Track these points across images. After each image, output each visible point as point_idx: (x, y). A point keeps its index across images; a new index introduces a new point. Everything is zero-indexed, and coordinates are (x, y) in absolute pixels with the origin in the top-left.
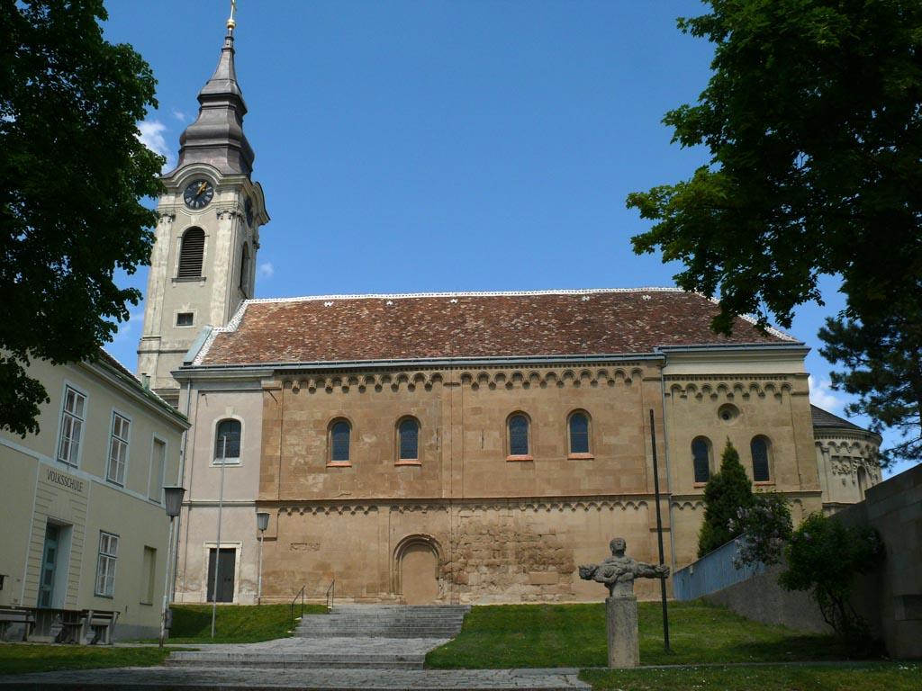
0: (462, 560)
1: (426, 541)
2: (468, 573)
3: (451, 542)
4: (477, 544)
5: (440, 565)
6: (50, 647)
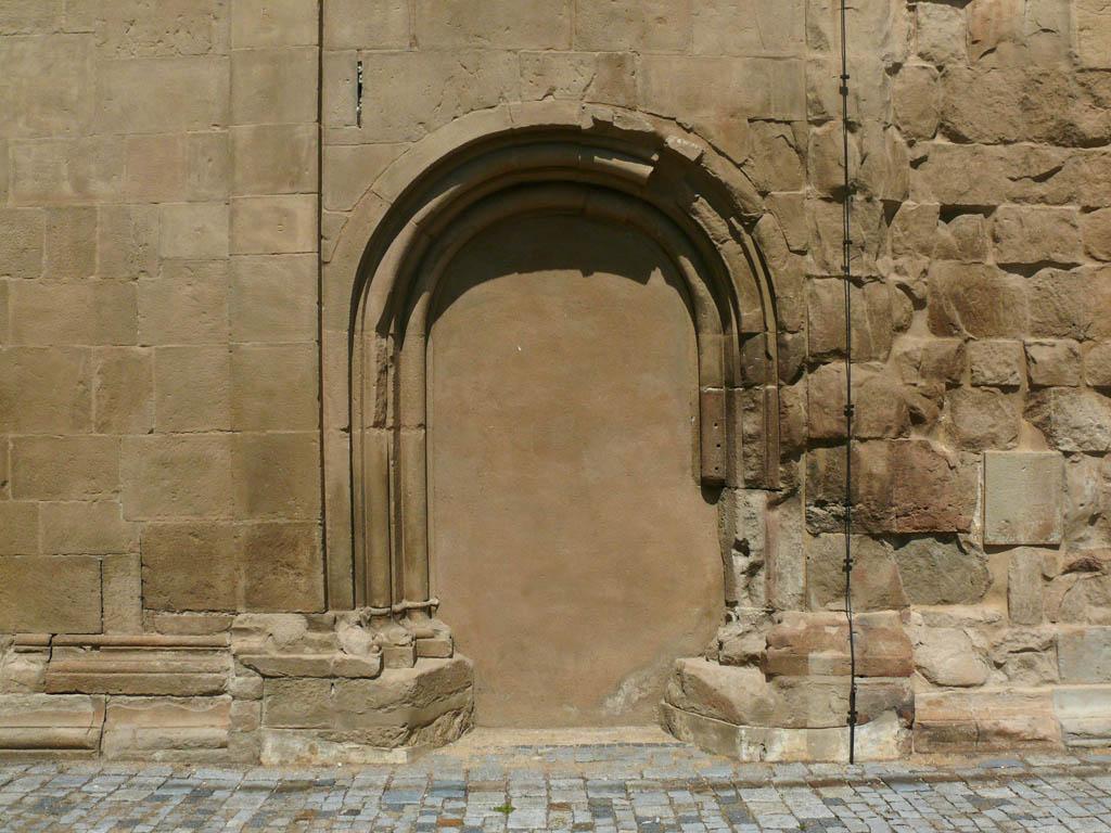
0: (918, 340)
1: (622, 188)
3: (840, 195)
4: (1035, 213)
5: (737, 380)
6: (150, 516)
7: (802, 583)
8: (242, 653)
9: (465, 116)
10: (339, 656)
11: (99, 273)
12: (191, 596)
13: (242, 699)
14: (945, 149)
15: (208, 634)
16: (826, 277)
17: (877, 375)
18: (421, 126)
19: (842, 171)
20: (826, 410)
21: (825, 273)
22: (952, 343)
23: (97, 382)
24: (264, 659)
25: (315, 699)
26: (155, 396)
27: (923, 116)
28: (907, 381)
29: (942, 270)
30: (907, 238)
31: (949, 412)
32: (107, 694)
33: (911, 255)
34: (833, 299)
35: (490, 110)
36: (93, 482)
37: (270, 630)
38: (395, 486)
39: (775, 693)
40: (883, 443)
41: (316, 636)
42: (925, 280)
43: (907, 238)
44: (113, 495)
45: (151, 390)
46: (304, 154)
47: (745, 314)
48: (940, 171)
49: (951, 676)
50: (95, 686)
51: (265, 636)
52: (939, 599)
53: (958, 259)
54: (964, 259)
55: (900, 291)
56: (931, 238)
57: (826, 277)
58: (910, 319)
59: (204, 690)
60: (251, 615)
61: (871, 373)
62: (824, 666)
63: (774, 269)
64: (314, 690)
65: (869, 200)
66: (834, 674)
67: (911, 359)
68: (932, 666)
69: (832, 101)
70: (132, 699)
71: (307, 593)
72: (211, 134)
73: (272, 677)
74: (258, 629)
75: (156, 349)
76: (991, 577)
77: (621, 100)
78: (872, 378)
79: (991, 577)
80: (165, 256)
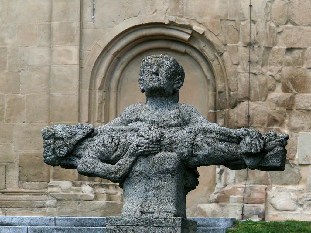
0: (278, 94)
2: (295, 130)
3: (250, 45)
7: (234, 175)
8: (52, 192)
9: (128, 19)
10: (81, 194)
11: (8, 69)
12: (35, 177)
13: (50, 207)
14: (290, 28)
15: (40, 189)
16: (244, 73)
17: (260, 105)
18: (113, 23)
19: (249, 37)
20: (242, 117)
21: (244, 72)
22: (289, 95)
23: (6, 106)
24: (57, 194)
25: (73, 207)
26: (25, 110)
27: (280, 17)
28: (272, 108)
29: (286, 70)
30: (274, 59)
31: (288, 119)
32: (7, 207)
33: (275, 65)
34: (246, 80)
35: (136, 17)
36: (4, 139)
37: (60, 186)
38: (205, 227)
39: (219, 208)
40: (262, 129)
41: (75, 188)
42: (280, 73)
43: (274, 59)
44: (11, 143)
45: (24, 109)
46: (75, 33)
47: (219, 85)
48: (287, 36)
49: (281, 207)
50: (3, 205)
51: (58, 188)
52: (283, 183)
53: (292, 66)
54: (294, 66)
55: (271, 77)
56: (282, 59)
57: (244, 73)
58: (275, 86)
59: (38, 206)
60: (54, 181)
61: (258, 105)
62: (234, 200)
63: (228, 70)
64: (73, 204)
65: (259, 47)
66: (238, 202)
67: (273, 101)
68: (276, 204)
69: (246, 11)
70: (14, 209)
71: (72, 174)
72: (45, 24)
73: (60, 200)
74: (56, 186)
75: (26, 95)
76: (301, 176)
77: (178, 14)
78: (258, 107)
79: (301, 176)
80: (30, 64)
